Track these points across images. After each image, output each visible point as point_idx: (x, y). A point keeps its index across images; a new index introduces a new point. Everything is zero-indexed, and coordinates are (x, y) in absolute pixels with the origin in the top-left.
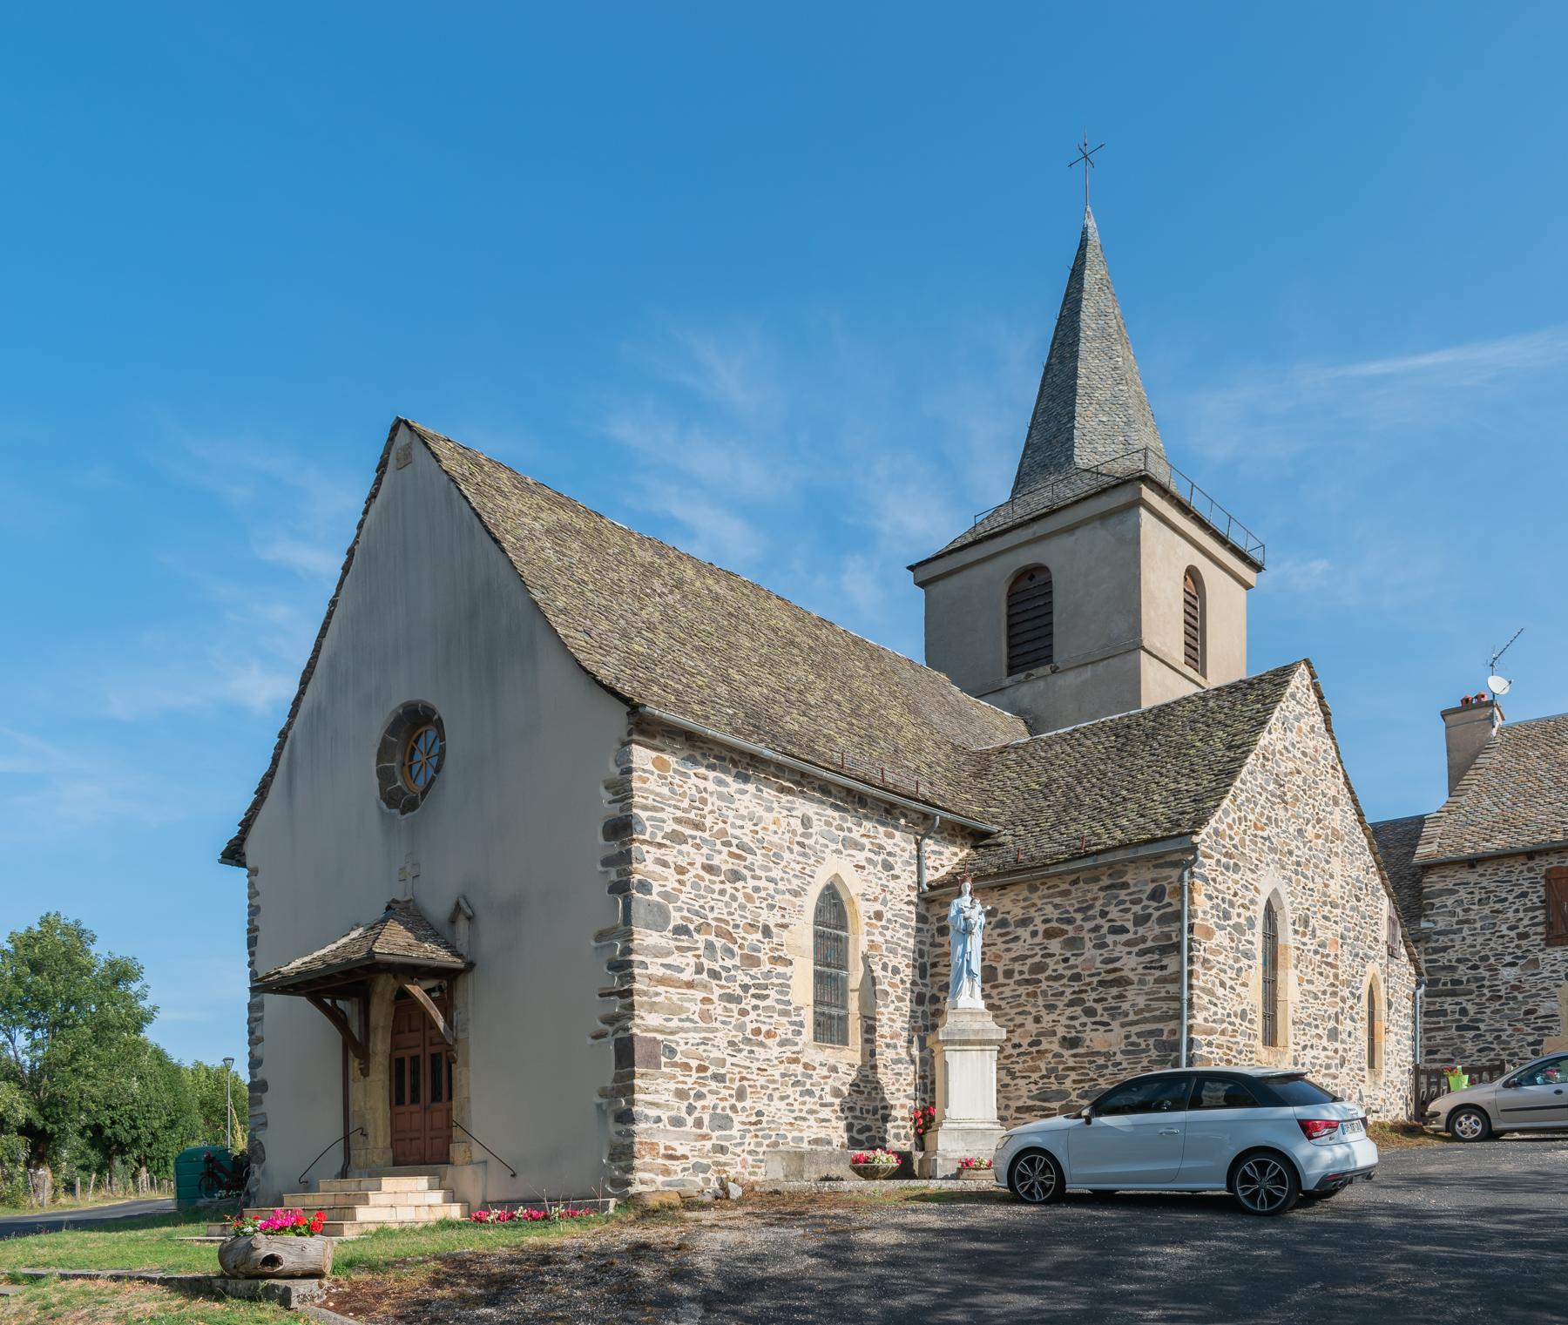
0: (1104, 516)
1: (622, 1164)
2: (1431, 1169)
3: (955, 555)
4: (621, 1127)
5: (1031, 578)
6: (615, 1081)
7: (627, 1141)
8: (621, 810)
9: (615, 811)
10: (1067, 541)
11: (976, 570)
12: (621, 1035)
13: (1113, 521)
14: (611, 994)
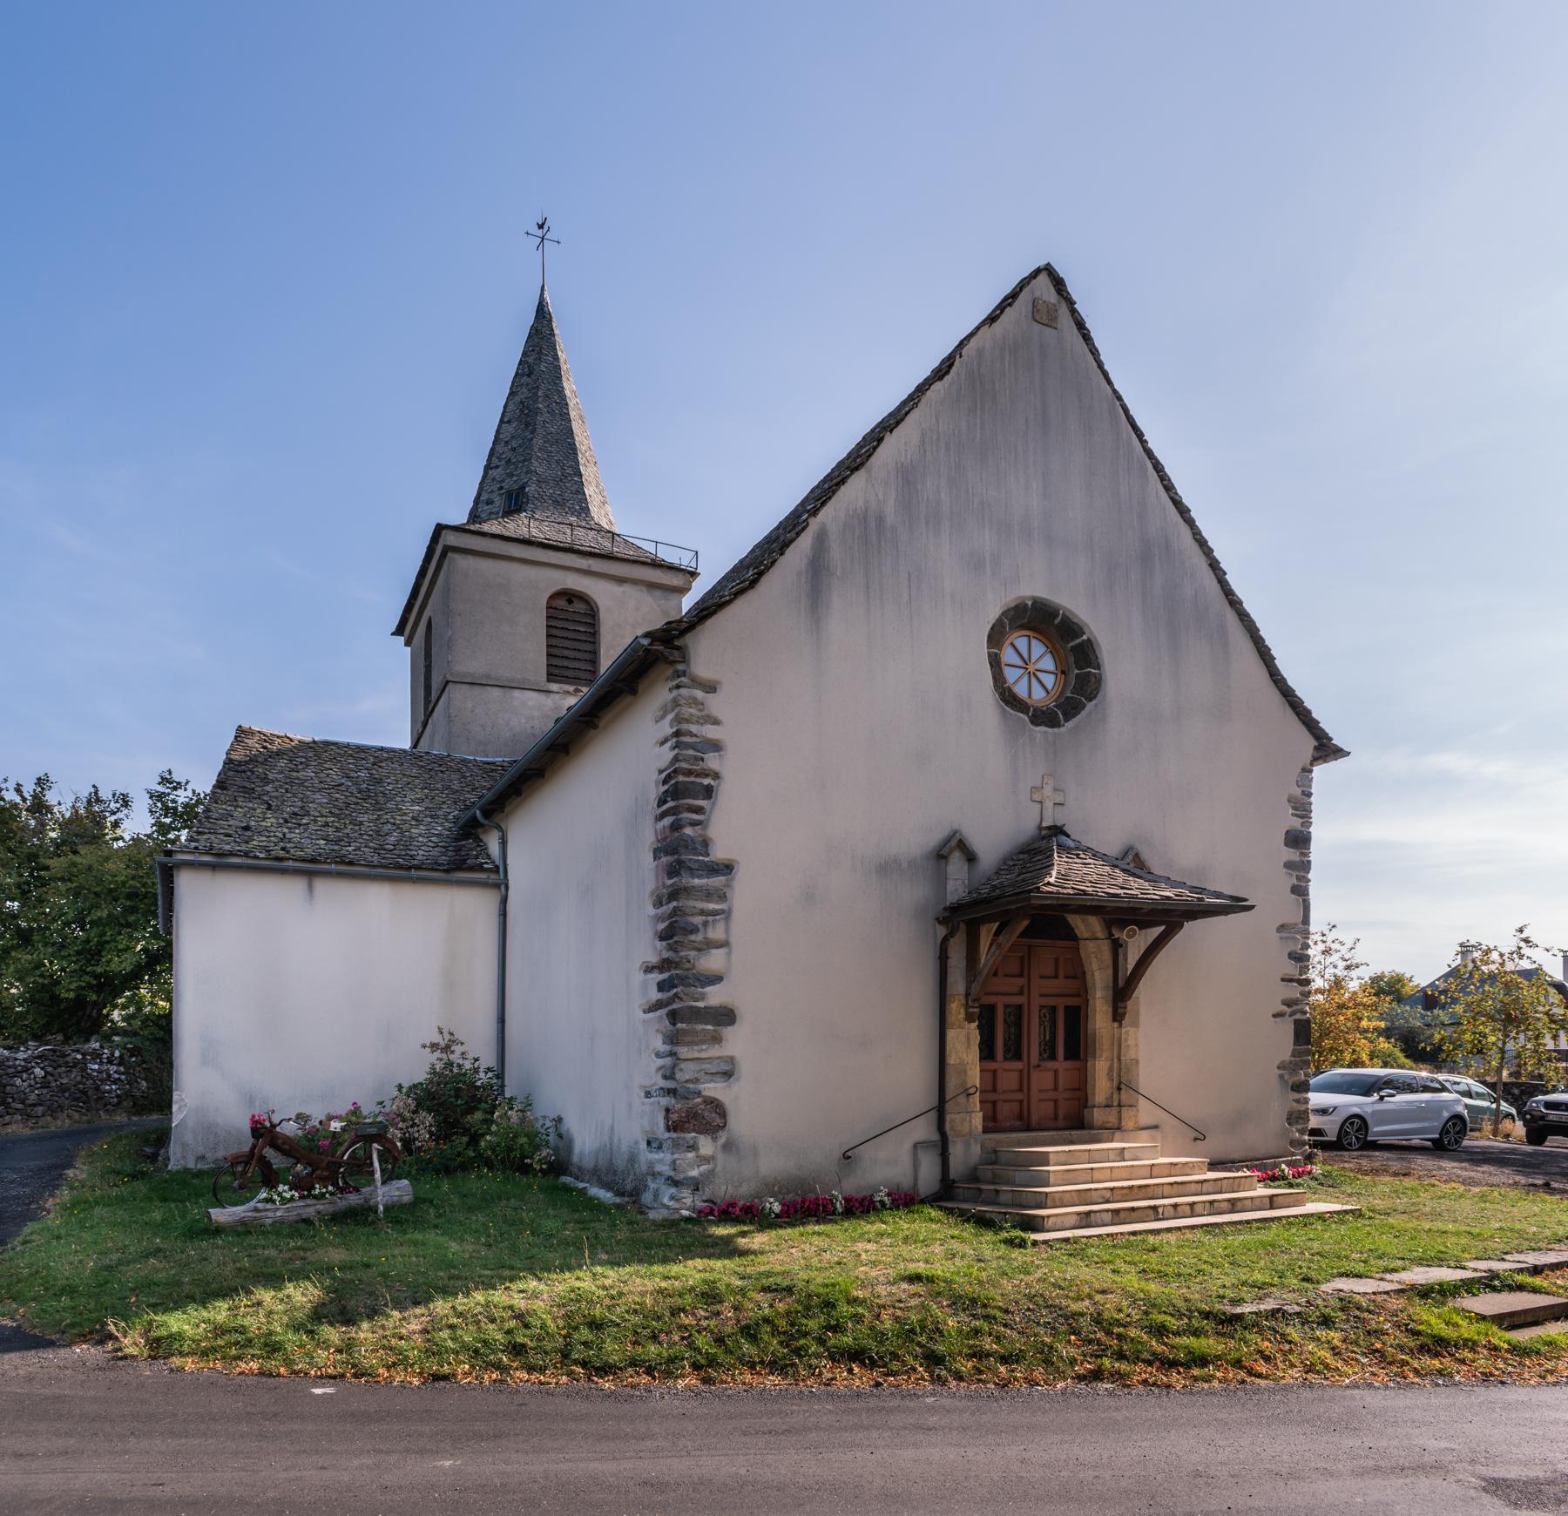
0: (652, 586)
1: (1299, 1127)
2: (1054, 1133)
3: (497, 541)
4: (1297, 1096)
5: (570, 602)
6: (1293, 1055)
7: (1303, 1108)
8: (1302, 824)
9: (1296, 823)
10: (617, 590)
11: (514, 566)
12: (1298, 1016)
13: (658, 593)
14: (1291, 980)
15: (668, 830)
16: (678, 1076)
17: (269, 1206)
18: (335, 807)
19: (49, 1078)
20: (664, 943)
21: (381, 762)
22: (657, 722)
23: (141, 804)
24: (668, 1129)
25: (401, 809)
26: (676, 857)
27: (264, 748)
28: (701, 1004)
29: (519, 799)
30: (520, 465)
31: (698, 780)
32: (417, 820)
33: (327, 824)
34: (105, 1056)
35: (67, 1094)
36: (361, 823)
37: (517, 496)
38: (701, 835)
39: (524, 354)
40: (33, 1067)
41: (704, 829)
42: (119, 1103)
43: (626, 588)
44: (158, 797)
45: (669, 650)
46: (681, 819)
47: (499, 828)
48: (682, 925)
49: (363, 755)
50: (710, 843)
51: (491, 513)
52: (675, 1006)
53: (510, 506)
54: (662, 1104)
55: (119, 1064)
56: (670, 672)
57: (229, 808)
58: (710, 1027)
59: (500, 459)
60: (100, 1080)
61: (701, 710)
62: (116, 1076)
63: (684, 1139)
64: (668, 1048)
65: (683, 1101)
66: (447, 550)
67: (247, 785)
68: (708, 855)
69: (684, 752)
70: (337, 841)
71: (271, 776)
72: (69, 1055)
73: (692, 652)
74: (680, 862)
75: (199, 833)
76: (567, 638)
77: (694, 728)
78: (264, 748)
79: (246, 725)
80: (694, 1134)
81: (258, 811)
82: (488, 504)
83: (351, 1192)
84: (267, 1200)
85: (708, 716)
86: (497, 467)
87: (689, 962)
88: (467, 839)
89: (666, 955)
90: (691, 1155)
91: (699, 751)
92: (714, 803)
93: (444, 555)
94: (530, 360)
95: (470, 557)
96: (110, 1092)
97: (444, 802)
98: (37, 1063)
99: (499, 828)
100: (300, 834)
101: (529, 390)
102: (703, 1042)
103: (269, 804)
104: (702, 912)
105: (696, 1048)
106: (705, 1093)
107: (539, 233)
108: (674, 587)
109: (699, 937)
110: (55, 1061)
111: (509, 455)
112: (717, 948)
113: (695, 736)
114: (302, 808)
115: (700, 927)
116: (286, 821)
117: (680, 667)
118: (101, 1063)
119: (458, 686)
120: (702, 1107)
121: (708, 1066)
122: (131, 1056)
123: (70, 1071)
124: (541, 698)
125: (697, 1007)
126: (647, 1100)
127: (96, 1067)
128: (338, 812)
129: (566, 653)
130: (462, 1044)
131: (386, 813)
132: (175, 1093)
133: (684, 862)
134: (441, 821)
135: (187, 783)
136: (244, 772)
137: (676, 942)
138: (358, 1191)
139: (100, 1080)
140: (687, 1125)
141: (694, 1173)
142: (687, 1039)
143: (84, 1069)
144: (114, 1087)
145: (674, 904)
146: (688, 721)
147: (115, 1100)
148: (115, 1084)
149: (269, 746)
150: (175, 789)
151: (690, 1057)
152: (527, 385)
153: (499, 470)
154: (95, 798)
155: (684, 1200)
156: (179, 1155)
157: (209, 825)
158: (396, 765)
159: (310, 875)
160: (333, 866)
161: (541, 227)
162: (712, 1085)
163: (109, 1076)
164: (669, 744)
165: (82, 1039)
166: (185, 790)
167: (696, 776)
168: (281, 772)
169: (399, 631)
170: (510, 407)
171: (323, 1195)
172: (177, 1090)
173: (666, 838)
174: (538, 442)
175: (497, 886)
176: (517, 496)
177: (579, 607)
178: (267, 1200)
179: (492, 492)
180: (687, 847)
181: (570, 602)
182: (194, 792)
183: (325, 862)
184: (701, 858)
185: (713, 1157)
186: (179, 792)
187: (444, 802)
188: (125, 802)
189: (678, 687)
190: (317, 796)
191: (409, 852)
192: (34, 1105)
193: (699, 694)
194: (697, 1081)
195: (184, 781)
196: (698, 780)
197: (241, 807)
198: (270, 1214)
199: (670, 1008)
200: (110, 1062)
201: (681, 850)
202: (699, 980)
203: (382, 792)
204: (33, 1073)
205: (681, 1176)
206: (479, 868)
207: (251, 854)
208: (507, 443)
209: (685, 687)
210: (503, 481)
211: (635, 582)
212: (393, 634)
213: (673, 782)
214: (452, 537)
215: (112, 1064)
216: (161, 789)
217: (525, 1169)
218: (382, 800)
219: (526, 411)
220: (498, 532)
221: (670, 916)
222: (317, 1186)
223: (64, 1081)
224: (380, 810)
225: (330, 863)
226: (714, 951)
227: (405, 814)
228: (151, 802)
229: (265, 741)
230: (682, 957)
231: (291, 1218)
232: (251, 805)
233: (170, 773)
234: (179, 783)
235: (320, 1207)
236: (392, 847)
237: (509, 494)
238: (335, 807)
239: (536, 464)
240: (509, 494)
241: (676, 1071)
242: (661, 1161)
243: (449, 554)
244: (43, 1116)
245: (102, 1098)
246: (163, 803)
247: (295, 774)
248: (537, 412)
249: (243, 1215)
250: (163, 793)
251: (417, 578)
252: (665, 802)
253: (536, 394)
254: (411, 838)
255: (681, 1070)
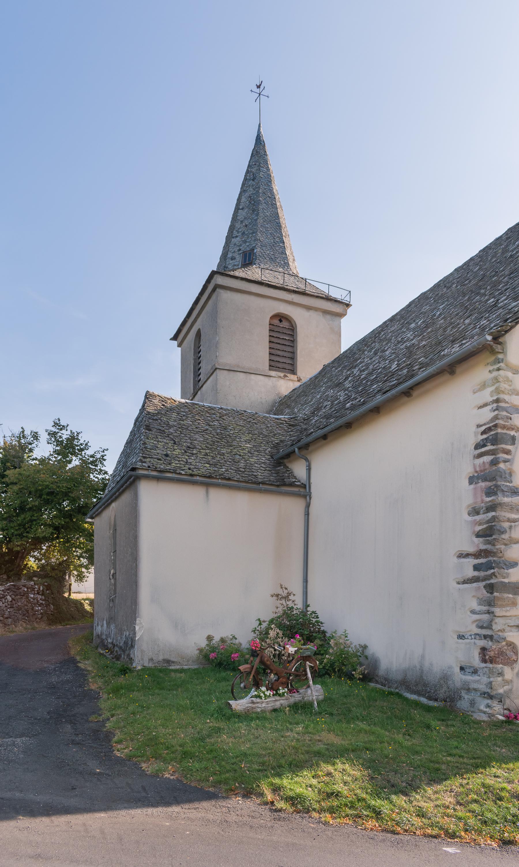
0: (326, 312)
11: (252, 298)
13: (328, 317)
15: (487, 466)
16: (494, 627)
17: (258, 700)
18: (208, 443)
19: (13, 601)
20: (481, 539)
21: (223, 416)
22: (474, 393)
23: (44, 437)
24: (484, 661)
25: (241, 446)
26: (494, 483)
27: (163, 405)
28: (506, 580)
29: (324, 441)
30: (250, 236)
31: (508, 432)
32: (251, 453)
33: (206, 454)
34: (36, 589)
35: (20, 612)
36: (223, 454)
37: (250, 254)
38: (509, 469)
39: (249, 166)
40: (7, 595)
41: (511, 465)
42: (42, 618)
43: (312, 313)
44: (53, 434)
45: (496, 345)
46: (499, 458)
47: (307, 460)
48: (498, 528)
49: (213, 412)
50: (513, 474)
51: (235, 265)
52: (492, 581)
53: (245, 261)
54: (478, 644)
55: (42, 595)
56: (492, 358)
57: (155, 442)
58: (511, 596)
59: (238, 232)
60: (34, 604)
61: (510, 386)
62: (41, 602)
63: (496, 668)
64: (485, 608)
65: (496, 644)
66: (217, 287)
67: (161, 428)
68: (512, 482)
69: (501, 413)
70: (215, 465)
71: (171, 423)
72: (21, 588)
73: (508, 346)
74: (497, 486)
75: (144, 457)
76: (279, 344)
77: (506, 397)
78: (163, 405)
79: (151, 391)
80: (501, 666)
81: (170, 445)
82: (232, 259)
83: (294, 692)
84: (256, 696)
85: (514, 390)
86: (237, 237)
87: (501, 552)
88: (280, 466)
89: (483, 547)
90: (500, 679)
91: (509, 413)
92: (517, 448)
93: (214, 290)
94: (254, 170)
95: (228, 292)
96: (38, 611)
97: (262, 443)
98: (8, 593)
99: (307, 460)
100: (194, 460)
101: (254, 189)
102: (507, 605)
103: (174, 440)
104: (509, 520)
105: (504, 609)
106: (508, 639)
107: (258, 91)
108: (338, 313)
109: (505, 536)
110: (15, 592)
111: (243, 229)
112: (515, 543)
113: (507, 403)
114: (191, 443)
115: (507, 529)
116: (186, 452)
117: (500, 356)
118: (34, 594)
119: (222, 371)
120: (506, 648)
121: (510, 621)
122: (47, 590)
123: (22, 598)
124: (266, 379)
125: (504, 582)
126: (460, 641)
127: (32, 596)
128: (210, 447)
129: (279, 353)
130: (294, 595)
131: (234, 448)
132: (138, 619)
133: (500, 486)
134: (263, 454)
135: (68, 425)
136: (157, 420)
137: (494, 539)
138: (298, 692)
139: (34, 604)
140: (498, 660)
141: (501, 691)
142: (500, 603)
143: (27, 597)
144: (39, 608)
145: (493, 514)
146: (503, 392)
147: (40, 616)
148: (40, 606)
149: (166, 405)
150: (61, 429)
151: (501, 615)
152: (253, 186)
153: (238, 238)
154: (23, 435)
155: (494, 708)
156: (140, 657)
157: (148, 453)
158: (231, 419)
159: (207, 485)
160: (220, 481)
161: (259, 87)
162: (511, 634)
163: (38, 601)
164: (489, 408)
165: (16, 579)
166: (67, 430)
167: (507, 430)
168: (175, 421)
169: (175, 338)
170: (243, 199)
171: (283, 693)
172: (138, 617)
173: (485, 470)
174: (260, 221)
175: (305, 497)
176: (250, 254)
177: (285, 324)
178: (256, 696)
179: (234, 252)
180: (501, 477)
181: (281, 321)
182: (71, 431)
183: (216, 478)
184: (508, 484)
185: (511, 681)
186: (63, 431)
187: (262, 443)
188: (36, 436)
189: (499, 369)
190: (197, 436)
191: (253, 473)
192: (7, 618)
193: (510, 374)
194: (503, 631)
195: (66, 425)
196: (508, 432)
197: (160, 442)
198: (259, 705)
199: (488, 582)
200: (38, 593)
201: (498, 478)
202: (505, 564)
203: (228, 435)
204: (6, 599)
205: (493, 693)
206: (292, 485)
207: (178, 472)
208: (242, 222)
209: (503, 370)
210: (241, 245)
211: (316, 309)
212: (171, 339)
213: (492, 433)
214: (220, 279)
215: (39, 595)
216: (54, 429)
217: (351, 677)
218: (230, 440)
219: (253, 202)
220: (244, 277)
221: (488, 522)
222: (281, 688)
223: (19, 604)
224: (231, 446)
225: (218, 479)
226: (514, 546)
227: (244, 449)
228: (48, 437)
229: (162, 401)
230: (497, 549)
231: (269, 708)
232: (165, 441)
233: (59, 420)
234: (63, 426)
235: (282, 702)
236: (244, 470)
237: (245, 254)
238: (208, 443)
239: (260, 235)
240: (245, 254)
241: (493, 624)
242: (478, 682)
243: (218, 290)
244: (11, 624)
245: (34, 614)
246: (55, 438)
247: (182, 422)
248: (258, 203)
249: (247, 705)
250: (55, 432)
251: (193, 305)
252: (484, 446)
253: (258, 192)
254: (251, 464)
255: (496, 623)
